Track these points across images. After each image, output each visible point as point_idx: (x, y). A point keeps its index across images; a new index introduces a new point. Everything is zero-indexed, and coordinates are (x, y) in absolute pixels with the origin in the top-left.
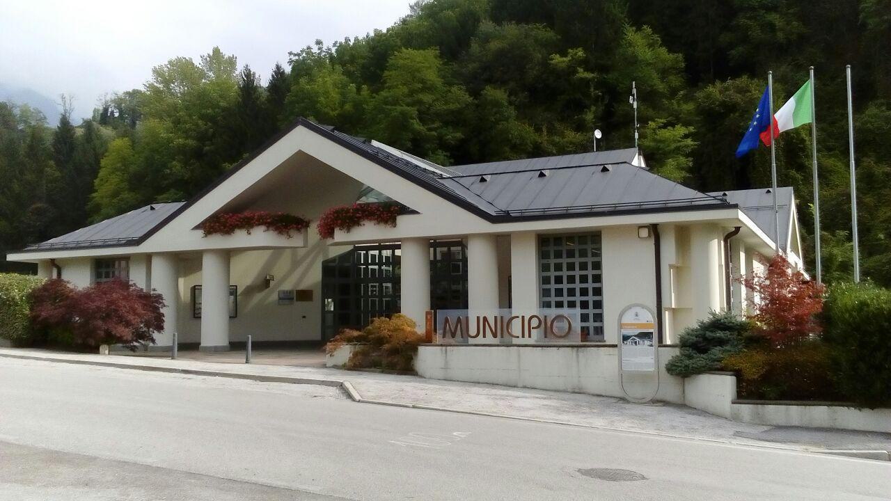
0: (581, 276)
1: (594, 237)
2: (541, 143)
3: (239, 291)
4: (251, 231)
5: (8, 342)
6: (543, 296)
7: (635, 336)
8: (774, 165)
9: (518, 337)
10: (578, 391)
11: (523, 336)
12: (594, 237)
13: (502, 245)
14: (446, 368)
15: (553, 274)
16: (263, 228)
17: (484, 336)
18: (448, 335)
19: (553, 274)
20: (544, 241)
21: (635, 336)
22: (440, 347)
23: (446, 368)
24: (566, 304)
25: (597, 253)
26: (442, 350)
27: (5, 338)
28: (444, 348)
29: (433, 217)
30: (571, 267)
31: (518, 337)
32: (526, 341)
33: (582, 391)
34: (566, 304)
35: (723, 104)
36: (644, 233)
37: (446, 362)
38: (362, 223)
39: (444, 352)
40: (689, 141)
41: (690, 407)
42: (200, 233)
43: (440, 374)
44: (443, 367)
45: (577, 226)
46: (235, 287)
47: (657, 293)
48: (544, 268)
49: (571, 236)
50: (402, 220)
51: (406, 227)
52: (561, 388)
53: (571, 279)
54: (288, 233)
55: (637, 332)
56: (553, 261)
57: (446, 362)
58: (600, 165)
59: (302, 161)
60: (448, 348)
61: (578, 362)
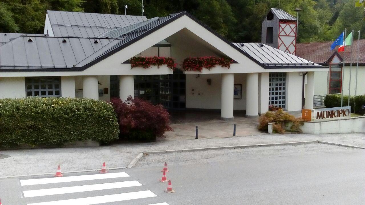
1: (284, 76)
4: (160, 66)
6: (28, 89)
8: (180, 13)
10: (353, 133)
12: (285, 74)
14: (320, 130)
20: (271, 75)
22: (319, 123)
23: (320, 130)
24: (40, 93)
25: (285, 80)
28: (320, 123)
34: (40, 93)
36: (302, 74)
37: (320, 128)
38: (215, 66)
41: (303, 133)
42: (129, 66)
43: (318, 132)
49: (277, 74)
50: (232, 65)
51: (234, 69)
52: (349, 131)
53: (277, 94)
54: (158, 66)
57: (320, 128)
58: (294, 40)
60: (321, 123)
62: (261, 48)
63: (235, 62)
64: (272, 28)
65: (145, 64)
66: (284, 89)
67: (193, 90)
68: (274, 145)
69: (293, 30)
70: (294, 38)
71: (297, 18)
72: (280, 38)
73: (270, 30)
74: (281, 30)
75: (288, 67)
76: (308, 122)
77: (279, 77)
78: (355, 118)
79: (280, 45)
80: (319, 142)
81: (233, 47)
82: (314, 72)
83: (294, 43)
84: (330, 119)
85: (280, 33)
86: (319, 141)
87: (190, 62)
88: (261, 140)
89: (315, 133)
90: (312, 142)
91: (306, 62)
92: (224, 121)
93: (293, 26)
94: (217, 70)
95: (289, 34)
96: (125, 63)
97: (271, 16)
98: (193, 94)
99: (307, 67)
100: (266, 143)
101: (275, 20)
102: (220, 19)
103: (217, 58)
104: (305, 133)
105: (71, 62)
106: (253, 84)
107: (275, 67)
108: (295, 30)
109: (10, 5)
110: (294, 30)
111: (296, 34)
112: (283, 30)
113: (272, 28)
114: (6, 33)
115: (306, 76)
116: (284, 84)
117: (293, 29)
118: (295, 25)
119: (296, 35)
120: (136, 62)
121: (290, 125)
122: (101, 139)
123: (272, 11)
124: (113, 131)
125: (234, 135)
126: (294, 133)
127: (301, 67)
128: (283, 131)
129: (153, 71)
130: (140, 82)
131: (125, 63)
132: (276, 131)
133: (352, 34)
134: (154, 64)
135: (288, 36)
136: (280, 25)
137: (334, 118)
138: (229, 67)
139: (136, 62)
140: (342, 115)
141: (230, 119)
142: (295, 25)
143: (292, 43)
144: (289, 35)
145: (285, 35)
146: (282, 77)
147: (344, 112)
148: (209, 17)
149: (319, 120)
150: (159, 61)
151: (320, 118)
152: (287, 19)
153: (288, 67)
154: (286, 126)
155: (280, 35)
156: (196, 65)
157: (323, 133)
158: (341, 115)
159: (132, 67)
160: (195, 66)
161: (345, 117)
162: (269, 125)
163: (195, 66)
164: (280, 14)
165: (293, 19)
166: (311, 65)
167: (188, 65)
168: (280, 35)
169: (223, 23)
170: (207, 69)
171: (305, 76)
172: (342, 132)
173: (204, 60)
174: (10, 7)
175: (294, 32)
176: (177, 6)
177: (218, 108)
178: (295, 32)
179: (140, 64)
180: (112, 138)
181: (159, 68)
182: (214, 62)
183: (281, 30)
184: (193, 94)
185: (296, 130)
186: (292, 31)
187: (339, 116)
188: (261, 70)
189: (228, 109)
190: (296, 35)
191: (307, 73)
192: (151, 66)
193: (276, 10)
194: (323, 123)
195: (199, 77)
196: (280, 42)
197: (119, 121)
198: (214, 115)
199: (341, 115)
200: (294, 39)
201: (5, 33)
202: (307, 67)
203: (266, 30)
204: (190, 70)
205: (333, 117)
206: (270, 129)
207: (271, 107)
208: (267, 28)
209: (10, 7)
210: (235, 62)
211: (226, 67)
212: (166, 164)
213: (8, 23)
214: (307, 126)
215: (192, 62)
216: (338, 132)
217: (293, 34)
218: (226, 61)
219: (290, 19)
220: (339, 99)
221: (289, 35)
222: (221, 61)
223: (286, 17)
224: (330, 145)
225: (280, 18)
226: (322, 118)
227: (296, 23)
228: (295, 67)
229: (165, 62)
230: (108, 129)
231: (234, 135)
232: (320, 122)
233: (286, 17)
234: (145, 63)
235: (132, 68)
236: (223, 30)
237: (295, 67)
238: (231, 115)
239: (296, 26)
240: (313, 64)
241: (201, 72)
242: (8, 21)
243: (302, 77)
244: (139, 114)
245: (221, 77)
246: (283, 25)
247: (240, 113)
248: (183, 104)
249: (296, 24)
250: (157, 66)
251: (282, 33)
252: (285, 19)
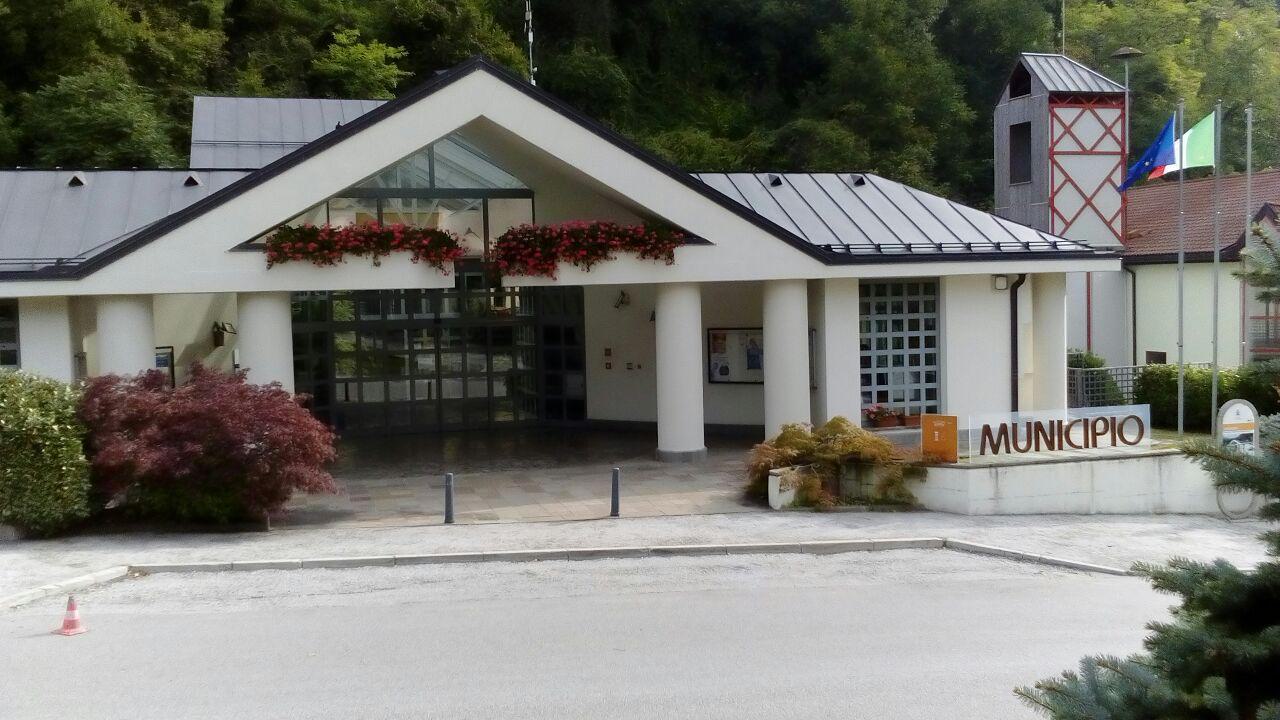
0: (911, 339)
2: (147, 41)
3: (177, 357)
4: (381, 259)
5: (10, 532)
7: (1237, 439)
9: (1080, 447)
10: (1161, 513)
11: (1087, 446)
12: (932, 286)
13: (815, 290)
15: (874, 335)
16: (409, 255)
17: (1037, 449)
18: (988, 450)
19: (874, 335)
20: (866, 287)
21: (1237, 439)
22: (987, 470)
23: (997, 497)
25: (933, 306)
26: (990, 473)
27: (11, 521)
28: (993, 470)
29: (729, 252)
30: (898, 325)
31: (1080, 447)
32: (1092, 452)
33: (1163, 511)
35: (427, 19)
36: (1002, 283)
39: (994, 475)
40: (394, 70)
42: (258, 259)
43: (987, 506)
44: (993, 497)
45: (925, 274)
46: (170, 350)
47: (1016, 359)
48: (865, 327)
49: (898, 286)
50: (683, 253)
51: (690, 265)
54: (375, 257)
55: (1238, 433)
56: (874, 317)
59: (481, 135)
60: (1000, 469)
61: (1160, 474)
62: (857, 190)
63: (691, 239)
64: (1029, 123)
65: (315, 250)
66: (931, 342)
67: (608, 352)
68: (725, 551)
69: (1109, 131)
70: (1118, 158)
71: (1124, 85)
72: (1054, 162)
73: (1021, 133)
74: (1058, 130)
75: (940, 256)
76: (945, 464)
77: (905, 299)
78: (1168, 454)
79: (1059, 189)
80: (945, 545)
81: (688, 186)
82: (1065, 273)
83: (1118, 179)
84: (1045, 453)
85: (1054, 144)
86: (950, 539)
87: (515, 243)
88: (690, 533)
89: (972, 508)
90: (913, 542)
91: (1028, 235)
92: (658, 465)
93: (1110, 115)
94: (622, 270)
95: (1092, 145)
96: (248, 246)
97: (1022, 81)
98: (609, 366)
99: (1027, 254)
100: (700, 543)
101: (1038, 96)
102: (902, 110)
103: (628, 223)
104: (927, 510)
105: (50, 252)
106: (785, 329)
107: (879, 257)
108: (1117, 131)
109: (167, 94)
110: (1062, 130)
111: (1122, 144)
112: (1068, 130)
113: (1029, 123)
114: (81, 175)
115: (1025, 294)
116: (931, 325)
117: (1109, 125)
118: (1118, 112)
119: (1123, 150)
120: (283, 245)
121: (874, 480)
122: (9, 513)
123: (1024, 64)
124: (60, 486)
125: (615, 512)
126: (883, 511)
127: (998, 255)
128: (828, 500)
129: (356, 274)
130: (312, 321)
131: (248, 246)
132: (807, 503)
133: (1216, 119)
134: (357, 251)
135: (1091, 152)
136: (1054, 115)
137: (1067, 453)
138: (670, 257)
139: (289, 243)
140: (1110, 441)
141: (686, 457)
142: (1118, 112)
143: (1109, 179)
144: (1096, 150)
145: (1078, 149)
146: (921, 299)
147: (1116, 429)
148: (864, 107)
149: (990, 457)
150: (375, 239)
151: (995, 450)
152: (1084, 89)
153: (940, 256)
154: (864, 481)
155: (1057, 149)
156: (534, 251)
157: (1007, 512)
158: (1105, 440)
159: (271, 263)
160: (531, 255)
161: (1122, 448)
162: (770, 477)
163: (531, 255)
164: (1054, 71)
165: (1107, 89)
166: (1046, 248)
167: (506, 255)
168: (1057, 149)
169: (917, 124)
170: (579, 268)
171: (1019, 289)
172: (1104, 508)
173: (560, 235)
174: (167, 101)
175: (1115, 139)
176: (756, 74)
177: (647, 419)
178: (1119, 135)
179: (299, 251)
180: (56, 511)
181: (377, 264)
182: (599, 241)
183: (1058, 130)
184: (609, 366)
185: (897, 501)
186: (1065, 133)
187: (1092, 439)
188: (815, 269)
189: (682, 419)
190: (1123, 150)
191: (1022, 277)
192: (349, 258)
193: (1041, 61)
194: (1010, 468)
195: (628, 303)
196: (1059, 179)
197: (89, 449)
198: (634, 441)
199: (1105, 440)
200: (1117, 166)
201: (69, 176)
202: (1027, 254)
203: (1006, 133)
204: (519, 272)
205: (1061, 448)
206: (777, 494)
207: (874, 413)
208: (1013, 128)
209: (167, 101)
210: (691, 239)
211: (656, 259)
212: (71, 606)
213: (148, 152)
214: (941, 483)
215: (521, 241)
216: (1084, 510)
217: (1110, 145)
218: (659, 237)
219: (1096, 89)
220: (1148, 377)
221: (1096, 150)
222: (631, 237)
223: (1079, 82)
224: (985, 558)
225: (1051, 88)
226: (1008, 451)
227: (1123, 103)
228: (969, 255)
229: (399, 243)
230: (39, 477)
231: (615, 512)
232: (991, 466)
233: (1079, 82)
234: (316, 245)
235: (270, 267)
236: (919, 149)
237: (969, 255)
238: (695, 442)
239: (1123, 116)
240: (1054, 245)
241: (555, 279)
242: (150, 143)
243: (1006, 297)
244: (183, 428)
245: (654, 291)
246: (1067, 114)
247: (728, 437)
248: (579, 406)
249: (1124, 109)
250: (371, 257)
251: (1067, 144)
252: (1073, 89)
